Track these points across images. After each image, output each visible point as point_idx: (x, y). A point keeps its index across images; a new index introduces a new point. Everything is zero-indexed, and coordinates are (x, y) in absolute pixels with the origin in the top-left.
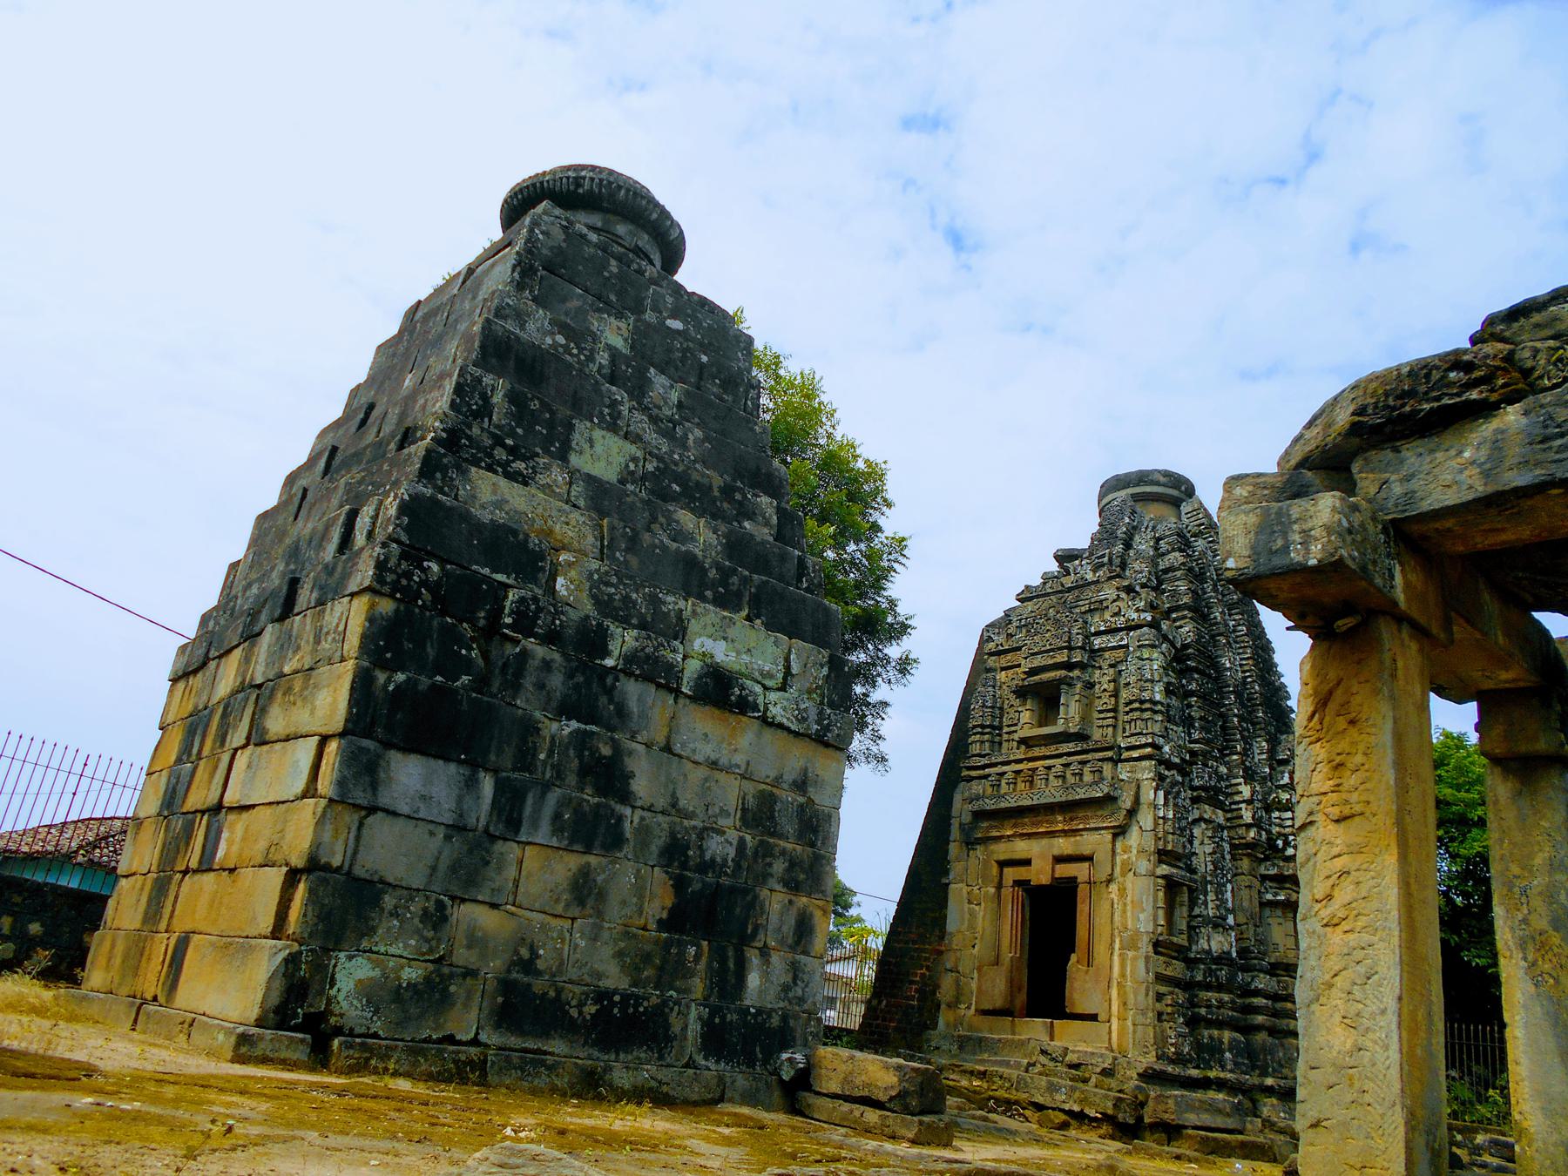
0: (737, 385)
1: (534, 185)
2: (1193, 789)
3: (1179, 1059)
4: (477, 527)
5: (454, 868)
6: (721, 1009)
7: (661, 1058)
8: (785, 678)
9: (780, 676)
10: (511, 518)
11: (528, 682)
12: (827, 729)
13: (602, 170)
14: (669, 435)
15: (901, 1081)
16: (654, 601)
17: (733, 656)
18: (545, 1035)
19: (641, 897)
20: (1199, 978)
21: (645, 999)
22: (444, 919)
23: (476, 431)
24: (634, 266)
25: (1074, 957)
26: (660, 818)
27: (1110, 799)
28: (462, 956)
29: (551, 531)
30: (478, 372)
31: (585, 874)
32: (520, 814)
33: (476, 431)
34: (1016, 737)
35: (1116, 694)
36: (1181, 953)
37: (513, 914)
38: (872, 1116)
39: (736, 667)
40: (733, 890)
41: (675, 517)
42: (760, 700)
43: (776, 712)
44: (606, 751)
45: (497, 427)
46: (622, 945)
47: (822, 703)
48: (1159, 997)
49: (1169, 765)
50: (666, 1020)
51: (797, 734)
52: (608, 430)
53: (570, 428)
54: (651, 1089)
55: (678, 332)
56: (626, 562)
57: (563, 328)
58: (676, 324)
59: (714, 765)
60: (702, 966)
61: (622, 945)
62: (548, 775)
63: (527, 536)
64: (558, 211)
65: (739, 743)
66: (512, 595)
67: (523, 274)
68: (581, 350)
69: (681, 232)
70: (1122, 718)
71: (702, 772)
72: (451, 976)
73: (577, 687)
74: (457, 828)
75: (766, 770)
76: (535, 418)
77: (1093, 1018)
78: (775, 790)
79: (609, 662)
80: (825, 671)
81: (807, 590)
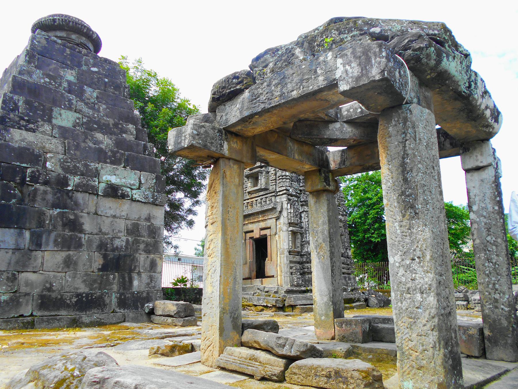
0: (120, 88)
1: (39, 23)
2: (301, 202)
3: (298, 285)
4: (13, 149)
5: (17, 262)
6: (123, 293)
7: (103, 311)
8: (139, 185)
9: (138, 185)
10: (28, 145)
11: (39, 198)
12: (156, 200)
13: (62, 15)
14: (93, 108)
15: (177, 308)
16: (86, 166)
17: (118, 180)
18: (58, 309)
19: (91, 262)
20: (305, 260)
21: (94, 294)
22: (16, 279)
23: (12, 116)
24: (77, 50)
25: (267, 259)
26: (96, 236)
27: (274, 209)
28: (24, 289)
29: (44, 147)
30: (11, 95)
31: (69, 257)
32: (41, 242)
33: (12, 116)
34: (247, 191)
35: (276, 175)
36: (299, 254)
37: (42, 274)
38: (170, 320)
39: (120, 184)
40: (125, 256)
41: (95, 136)
42: (130, 194)
43: (136, 197)
44: (72, 217)
45: (21, 113)
46: (85, 278)
47: (154, 192)
48: (291, 268)
49: (292, 195)
50: (104, 300)
51: (145, 203)
52: (67, 109)
53: (52, 110)
54: (97, 322)
55: (96, 72)
56: (75, 154)
57: (48, 76)
58: (95, 69)
59: (114, 217)
60: (116, 281)
61: (85, 278)
62: (51, 228)
63: (34, 150)
64: (43, 33)
65: (124, 208)
66: (29, 171)
67: (30, 58)
68: (56, 83)
69: (97, 35)
70: (278, 182)
71: (111, 219)
72: (20, 296)
73: (58, 198)
74: (17, 249)
75: (134, 216)
76: (37, 109)
77: (273, 276)
78: (138, 222)
79: (70, 188)
80: (154, 181)
81: (148, 155)
